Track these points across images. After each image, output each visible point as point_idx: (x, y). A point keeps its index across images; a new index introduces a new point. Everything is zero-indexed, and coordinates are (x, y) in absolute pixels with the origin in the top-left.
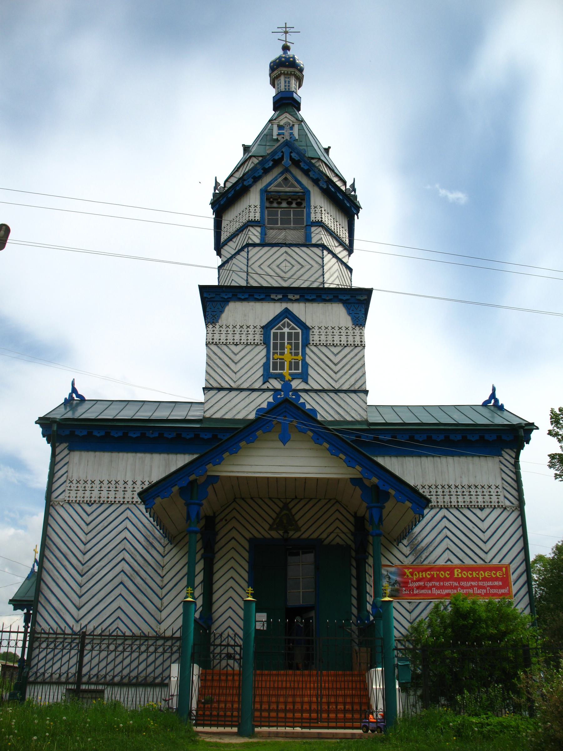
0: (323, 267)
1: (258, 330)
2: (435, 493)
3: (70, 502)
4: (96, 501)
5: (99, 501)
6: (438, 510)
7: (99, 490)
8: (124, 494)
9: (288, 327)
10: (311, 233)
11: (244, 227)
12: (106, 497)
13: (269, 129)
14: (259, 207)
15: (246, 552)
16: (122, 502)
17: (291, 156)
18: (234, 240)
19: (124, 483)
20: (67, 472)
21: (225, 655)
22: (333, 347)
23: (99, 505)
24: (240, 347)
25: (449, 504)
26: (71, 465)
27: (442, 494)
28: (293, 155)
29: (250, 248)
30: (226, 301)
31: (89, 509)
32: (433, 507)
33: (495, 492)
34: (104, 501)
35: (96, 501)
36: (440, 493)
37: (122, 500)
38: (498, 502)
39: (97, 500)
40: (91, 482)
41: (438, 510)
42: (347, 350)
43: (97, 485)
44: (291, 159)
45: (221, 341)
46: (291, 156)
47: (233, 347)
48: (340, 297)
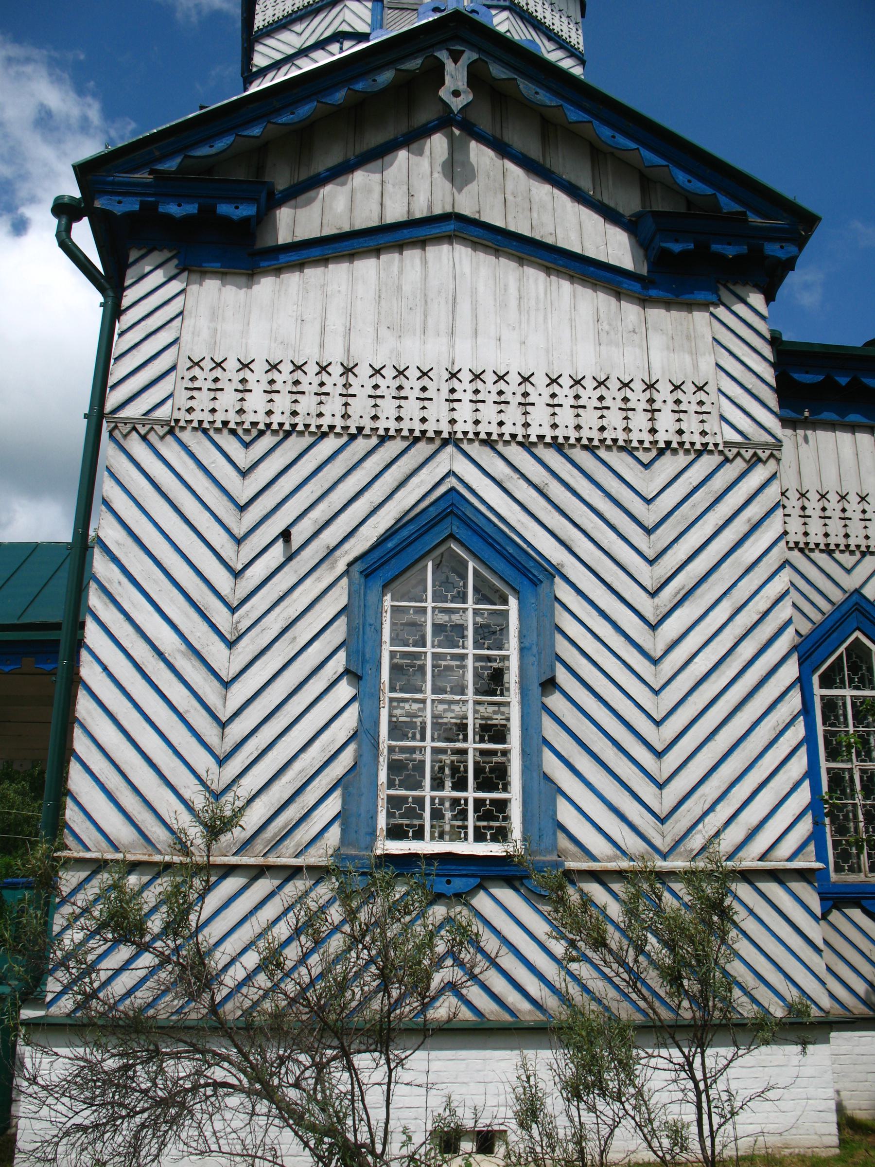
2: (470, 396)
3: (561, 440)
4: (334, 427)
5: (346, 428)
6: (308, 440)
7: (269, 389)
8: (626, 418)
12: (417, 417)
13: (316, 62)
15: (91, 646)
16: (417, 434)
19: (372, 372)
20: (176, 341)
23: (374, 441)
25: (647, 438)
26: (189, 322)
27: (572, 402)
32: (711, 447)
33: (290, 383)
34: (360, 429)
35: (334, 427)
36: (691, 407)
37: (446, 429)
38: (578, 427)
40: (317, 369)
41: (308, 440)
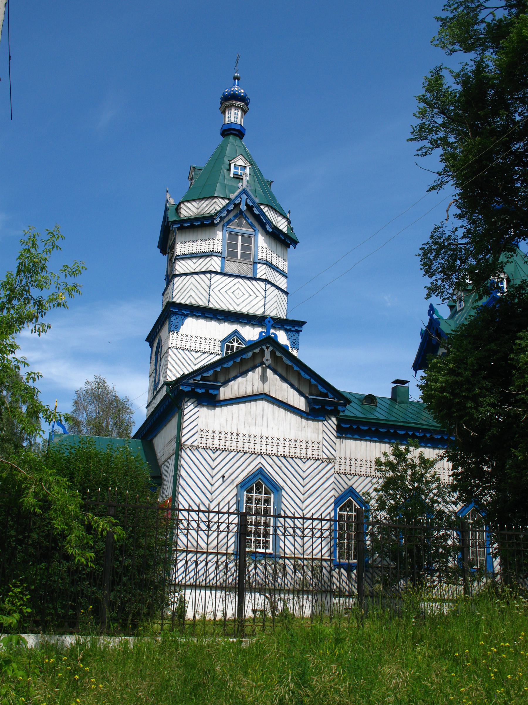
0: (265, 297)
1: (217, 343)
9: (237, 342)
10: (257, 269)
11: (204, 254)
14: (221, 240)
17: (246, 202)
18: (194, 260)
21: (316, 536)
22: (194, 353)
24: (199, 354)
28: (248, 201)
29: (213, 275)
30: (186, 316)
31: (214, 456)
37: (259, 451)
39: (235, 449)
42: (206, 355)
43: (258, 439)
44: (247, 205)
45: (192, 348)
46: (246, 202)
47: (194, 353)
48: (285, 327)
